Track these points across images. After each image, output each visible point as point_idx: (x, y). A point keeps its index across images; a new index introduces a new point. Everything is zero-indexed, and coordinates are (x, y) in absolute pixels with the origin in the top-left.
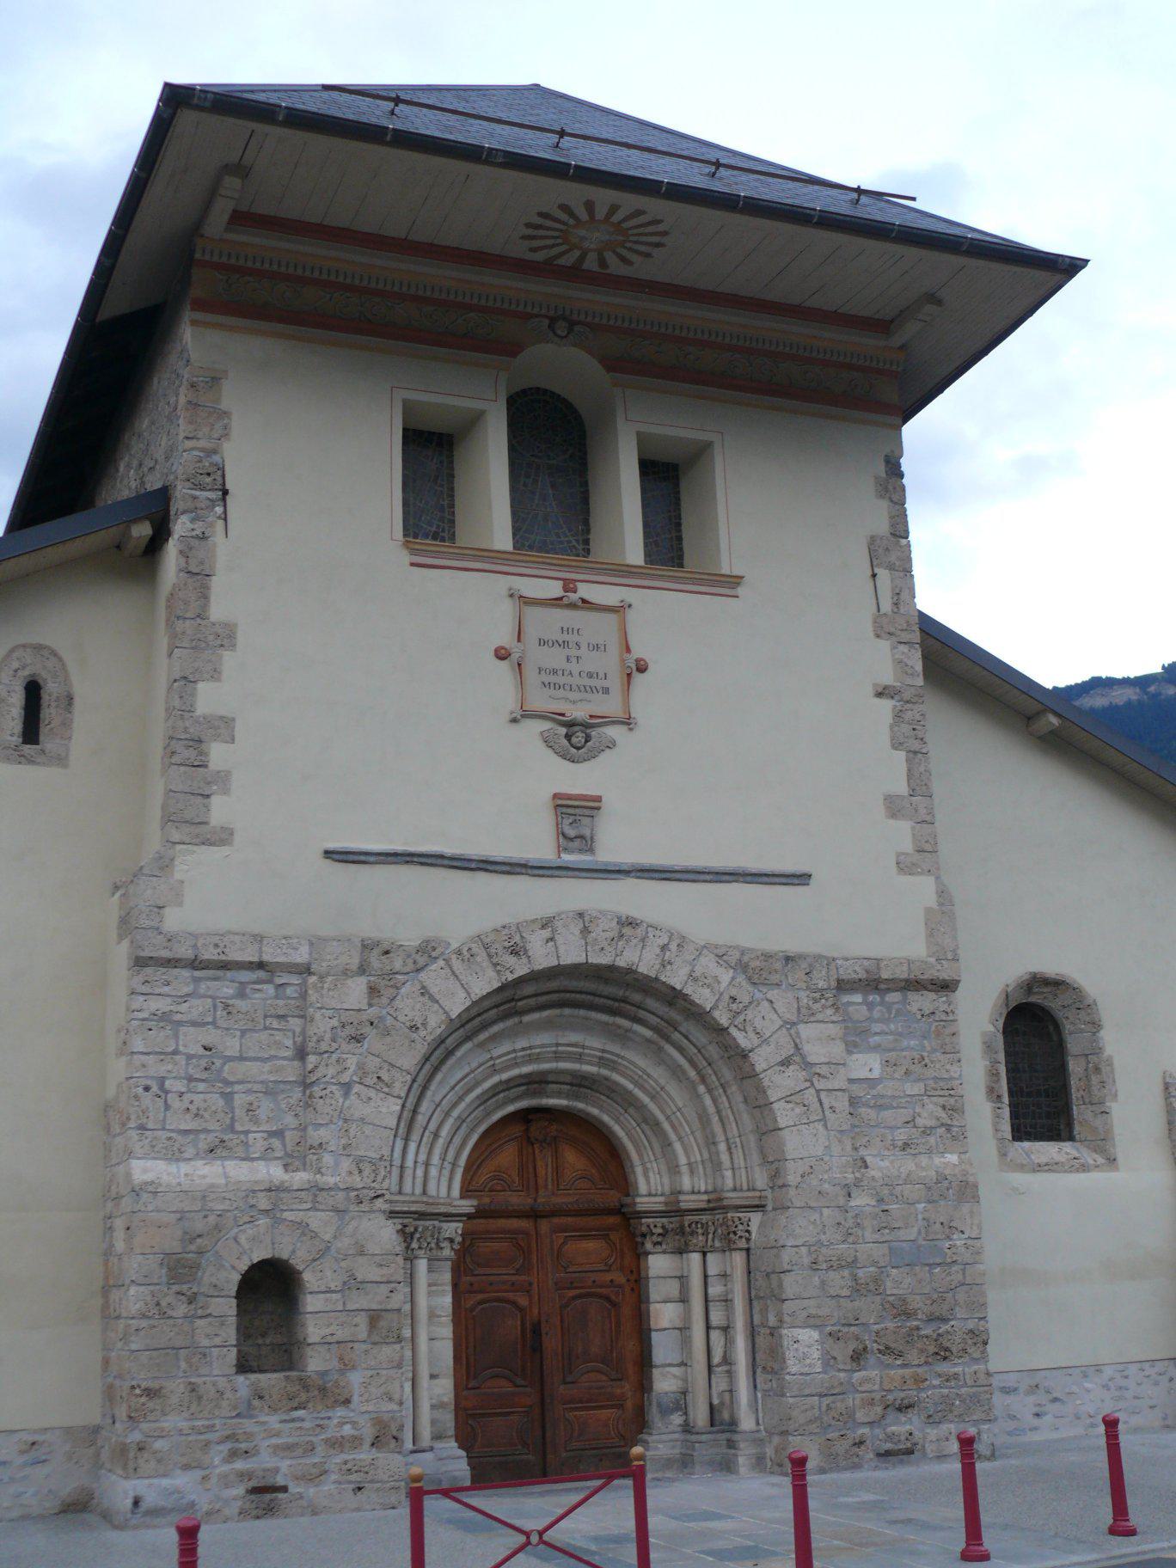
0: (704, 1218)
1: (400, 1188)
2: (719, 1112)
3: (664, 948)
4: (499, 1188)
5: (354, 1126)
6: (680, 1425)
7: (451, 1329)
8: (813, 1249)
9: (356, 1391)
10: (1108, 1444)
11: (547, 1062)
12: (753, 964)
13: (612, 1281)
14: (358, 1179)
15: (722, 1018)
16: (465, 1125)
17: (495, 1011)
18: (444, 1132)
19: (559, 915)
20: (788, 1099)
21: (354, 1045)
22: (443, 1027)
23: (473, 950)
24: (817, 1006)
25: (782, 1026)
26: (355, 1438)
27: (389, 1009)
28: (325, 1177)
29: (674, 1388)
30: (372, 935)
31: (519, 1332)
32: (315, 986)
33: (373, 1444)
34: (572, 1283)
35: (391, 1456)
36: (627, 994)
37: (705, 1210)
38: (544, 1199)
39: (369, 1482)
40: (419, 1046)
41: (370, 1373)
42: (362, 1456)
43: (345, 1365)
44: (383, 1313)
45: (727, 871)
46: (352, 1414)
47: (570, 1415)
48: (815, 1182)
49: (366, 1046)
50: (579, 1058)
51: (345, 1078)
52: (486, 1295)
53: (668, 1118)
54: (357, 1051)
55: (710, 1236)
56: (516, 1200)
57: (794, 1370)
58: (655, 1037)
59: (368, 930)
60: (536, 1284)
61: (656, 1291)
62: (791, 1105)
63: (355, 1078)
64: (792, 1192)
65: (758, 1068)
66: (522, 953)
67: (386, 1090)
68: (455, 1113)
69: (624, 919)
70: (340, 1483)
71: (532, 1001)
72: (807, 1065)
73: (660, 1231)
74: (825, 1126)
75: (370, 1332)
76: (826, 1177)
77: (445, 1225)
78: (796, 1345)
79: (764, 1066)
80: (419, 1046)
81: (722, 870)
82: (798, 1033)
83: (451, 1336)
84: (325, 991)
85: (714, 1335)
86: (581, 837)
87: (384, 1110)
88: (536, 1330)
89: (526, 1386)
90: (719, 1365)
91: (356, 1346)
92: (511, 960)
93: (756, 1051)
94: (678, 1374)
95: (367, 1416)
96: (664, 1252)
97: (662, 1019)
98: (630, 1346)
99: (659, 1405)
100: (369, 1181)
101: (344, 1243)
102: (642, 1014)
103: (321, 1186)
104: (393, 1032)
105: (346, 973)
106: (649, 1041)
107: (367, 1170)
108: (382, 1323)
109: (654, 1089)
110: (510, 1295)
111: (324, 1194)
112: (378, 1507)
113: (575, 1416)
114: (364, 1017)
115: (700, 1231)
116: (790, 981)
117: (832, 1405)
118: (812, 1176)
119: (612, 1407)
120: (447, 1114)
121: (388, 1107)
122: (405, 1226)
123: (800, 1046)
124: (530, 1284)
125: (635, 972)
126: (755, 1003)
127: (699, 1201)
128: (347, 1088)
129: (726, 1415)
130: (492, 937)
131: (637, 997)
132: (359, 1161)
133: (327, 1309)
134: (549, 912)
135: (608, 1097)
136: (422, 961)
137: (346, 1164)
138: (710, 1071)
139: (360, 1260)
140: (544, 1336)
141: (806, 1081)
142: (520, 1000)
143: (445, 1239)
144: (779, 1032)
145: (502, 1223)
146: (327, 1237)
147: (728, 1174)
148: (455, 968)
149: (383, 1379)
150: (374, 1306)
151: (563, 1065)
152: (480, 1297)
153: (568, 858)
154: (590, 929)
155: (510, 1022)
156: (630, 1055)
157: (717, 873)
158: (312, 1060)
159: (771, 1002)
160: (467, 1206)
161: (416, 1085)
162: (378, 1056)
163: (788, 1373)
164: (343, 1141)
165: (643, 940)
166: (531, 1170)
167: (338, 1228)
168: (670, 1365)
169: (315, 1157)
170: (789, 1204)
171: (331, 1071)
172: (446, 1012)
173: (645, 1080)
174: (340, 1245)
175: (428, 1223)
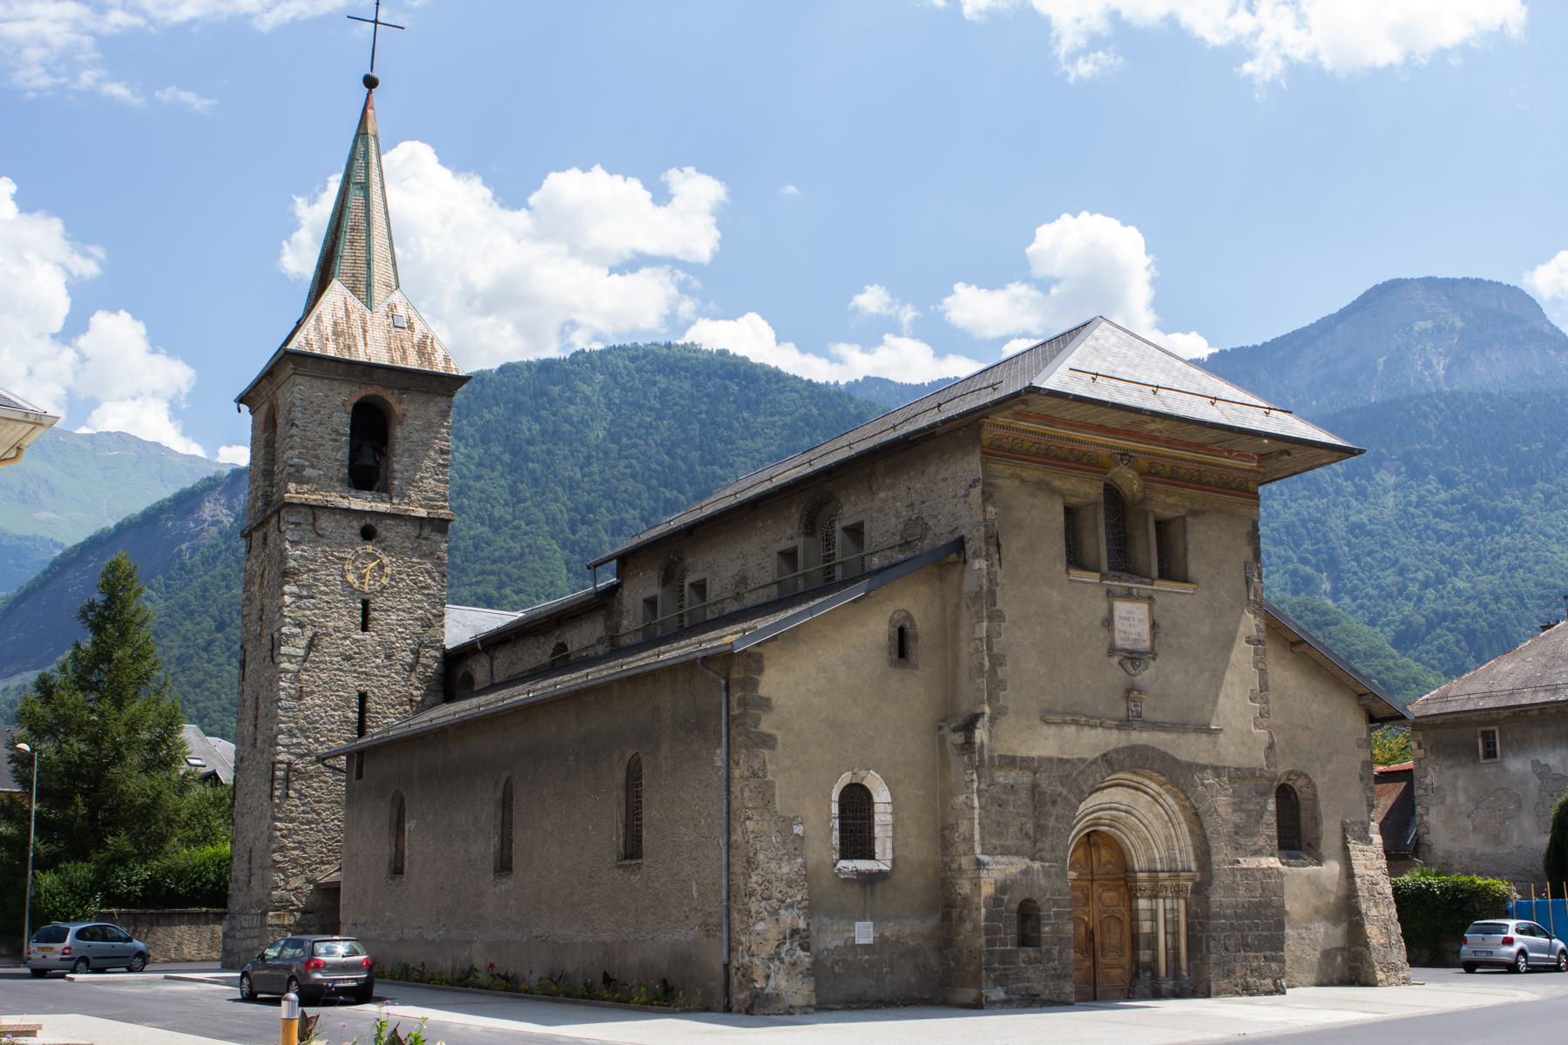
88: (1092, 933)
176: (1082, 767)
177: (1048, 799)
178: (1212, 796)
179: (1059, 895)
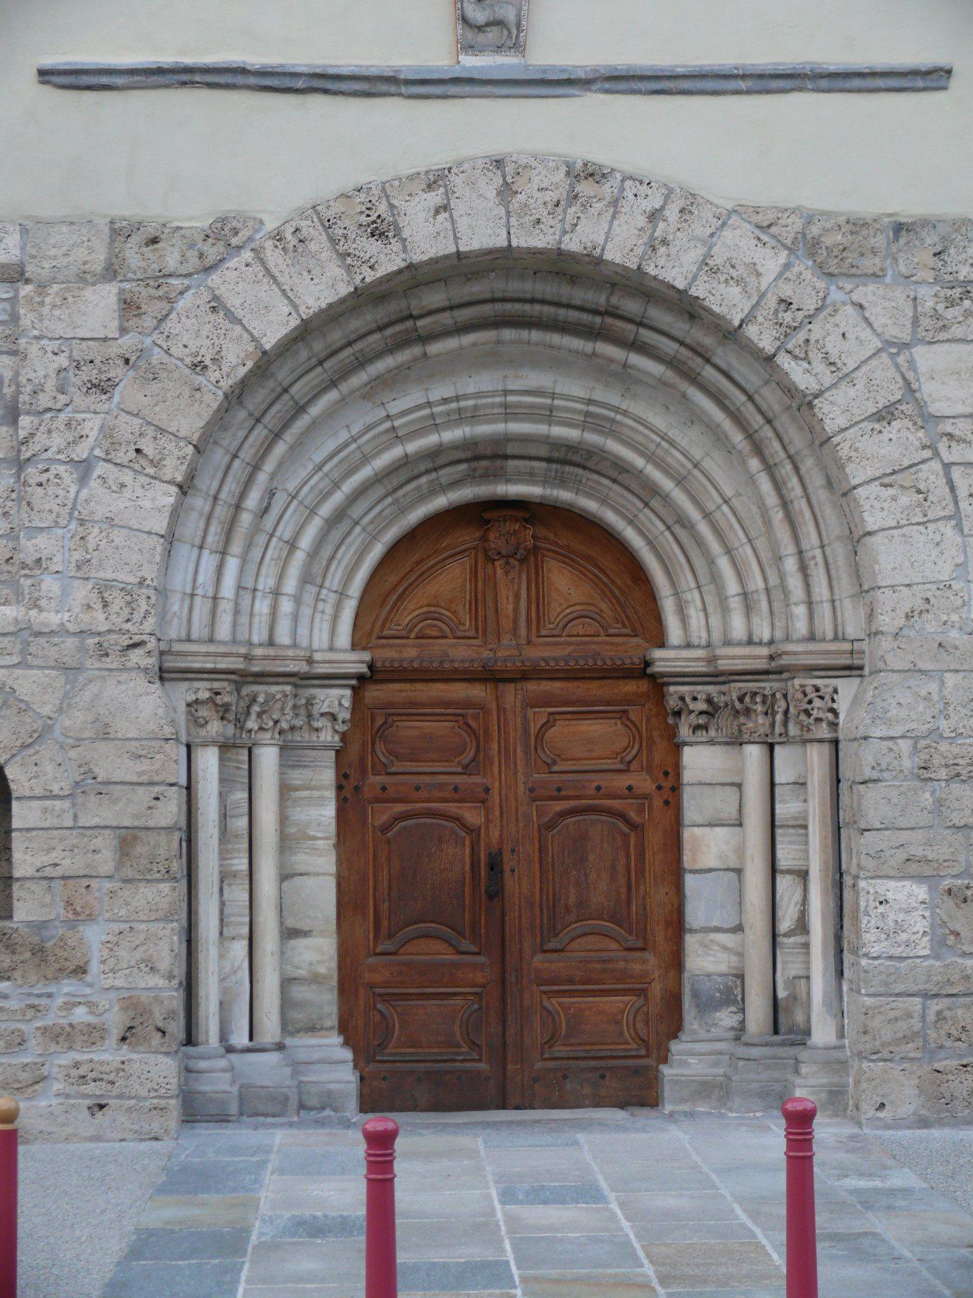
0: (768, 686)
1: (212, 631)
2: (785, 504)
3: (654, 216)
4: (435, 633)
5: (96, 531)
6: (733, 1028)
7: (333, 858)
8: (922, 743)
9: (96, 955)
10: (790, 1159)
11: (489, 422)
12: (828, 240)
13: (630, 788)
14: (102, 617)
15: (763, 336)
17: (377, 336)
19: (460, 164)
20: (887, 480)
21: (94, 399)
22: (250, 364)
23: (304, 231)
24: (950, 314)
25: (879, 351)
26: (92, 1028)
27: (155, 336)
28: (44, 615)
29: (723, 968)
30: (127, 212)
31: (468, 867)
32: (29, 300)
33: (124, 1039)
34: (559, 790)
35: (152, 1058)
36: (614, 300)
37: (767, 672)
38: (504, 652)
39: (117, 1097)
40: (208, 398)
41: (116, 927)
42: (106, 1057)
43: (76, 913)
44: (142, 834)
45: (781, 69)
46: (88, 991)
47: (553, 1003)
48: (930, 628)
49: (116, 399)
50: (549, 415)
51: (81, 452)
52: (408, 807)
53: (707, 516)
54: (100, 407)
55: (779, 717)
56: (461, 653)
57: (875, 950)
58: (670, 375)
59: (126, 209)
60: (496, 790)
61: (694, 806)
62: (891, 491)
63: (97, 452)
64: (886, 643)
65: (830, 427)
66: (390, 234)
67: (151, 471)
69: (579, 165)
70: (68, 1096)
71: (446, 319)
72: (926, 419)
73: (702, 706)
74: (959, 527)
75: (119, 865)
76: (955, 617)
77: (320, 693)
78: (881, 909)
79: (842, 421)
80: (208, 398)
81: (770, 70)
82: (911, 363)
83: (333, 869)
84: (46, 310)
85: (783, 883)
86: (499, 23)
87: (147, 504)
88: (495, 864)
89: (479, 954)
90: (788, 934)
91: (94, 883)
92: (371, 247)
93: (827, 395)
94: (730, 945)
95: (113, 995)
96: (712, 742)
97: (682, 343)
98: (659, 895)
99: (696, 995)
100: (120, 620)
101: (77, 719)
102: (647, 336)
103: (36, 628)
104: (163, 375)
105: (84, 278)
106: (662, 382)
107: (118, 601)
108: (139, 849)
109: (683, 466)
110: (451, 808)
111: (42, 640)
112: (130, 1136)
113: (560, 1004)
114: (113, 350)
115: (759, 708)
116: (902, 268)
117: (947, 1014)
118: (930, 616)
119: (625, 992)
121: (154, 499)
122: (217, 694)
123: (915, 386)
124: (487, 790)
125: (599, 261)
126: (829, 310)
127: (756, 657)
128: (84, 468)
129: (799, 1018)
130: (337, 208)
131: (631, 306)
132: (103, 588)
133: (46, 825)
134: (440, 159)
135: (614, 481)
136: (213, 253)
137: (81, 592)
138: (770, 434)
139: (102, 746)
140: (507, 875)
141: (924, 447)
142: (421, 317)
143: (322, 715)
144: (874, 362)
145: (438, 690)
146: (47, 710)
147: (800, 611)
148: (271, 264)
149: (142, 937)
150: (127, 822)
151: (516, 427)
152: (399, 808)
153: (473, 63)
154: (515, 187)
155: (404, 356)
156: (638, 408)
157: (761, 76)
158: (25, 421)
159: (861, 306)
160: (355, 662)
162: (137, 415)
163: (866, 955)
164: (77, 556)
165: (615, 203)
166: (490, 603)
167: (66, 695)
168: (717, 930)
169: (29, 582)
170: (881, 665)
171: (57, 441)
172: (254, 339)
173: (666, 451)
174: (67, 723)
175: (274, 689)
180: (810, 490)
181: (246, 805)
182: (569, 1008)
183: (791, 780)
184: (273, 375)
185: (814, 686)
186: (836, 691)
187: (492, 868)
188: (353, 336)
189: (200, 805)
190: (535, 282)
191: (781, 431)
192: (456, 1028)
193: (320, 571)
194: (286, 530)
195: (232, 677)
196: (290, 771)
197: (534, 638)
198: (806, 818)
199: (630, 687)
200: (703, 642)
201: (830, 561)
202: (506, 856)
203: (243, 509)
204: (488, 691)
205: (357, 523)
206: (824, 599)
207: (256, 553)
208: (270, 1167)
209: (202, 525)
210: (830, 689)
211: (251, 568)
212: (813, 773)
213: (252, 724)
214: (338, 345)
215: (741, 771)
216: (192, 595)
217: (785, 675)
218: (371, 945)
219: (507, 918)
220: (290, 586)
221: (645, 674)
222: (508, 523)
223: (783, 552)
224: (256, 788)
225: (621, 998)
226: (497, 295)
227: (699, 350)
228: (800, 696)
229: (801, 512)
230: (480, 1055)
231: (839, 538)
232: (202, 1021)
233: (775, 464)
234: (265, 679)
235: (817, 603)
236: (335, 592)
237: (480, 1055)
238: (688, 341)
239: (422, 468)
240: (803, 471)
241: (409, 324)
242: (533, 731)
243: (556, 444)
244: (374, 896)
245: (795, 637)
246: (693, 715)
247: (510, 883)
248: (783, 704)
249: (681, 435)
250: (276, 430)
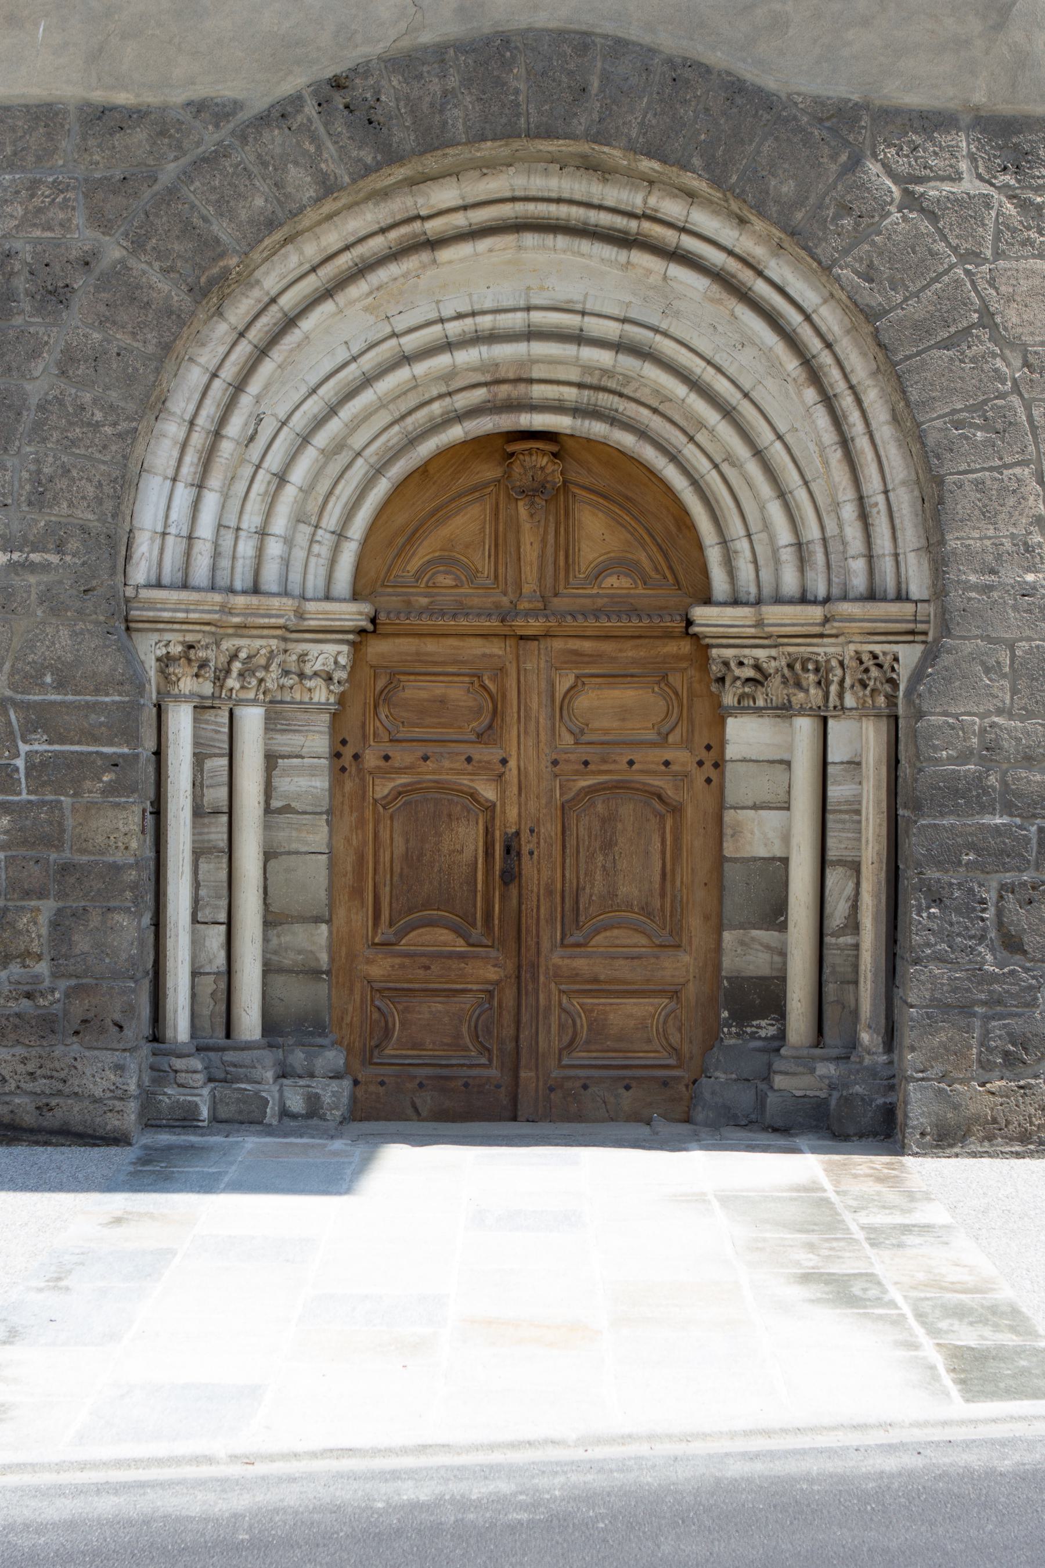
1: (187, 575)
16: (360, 461)
18: (298, 475)
36: (652, 201)
55: (834, 689)
68: (321, 439)
71: (459, 221)
73: (750, 673)
77: (314, 649)
85: (833, 877)
90: (842, 931)
115: (812, 677)
120: (305, 440)
122: (191, 647)
124: (504, 762)
135: (655, 411)
140: (525, 857)
143: (316, 674)
161: (217, 384)
176: (211, 138)
177: (21, 284)
178: (973, 256)
179: (60, 685)
180: (874, 425)
181: (226, 773)
182: (592, 1011)
183: (845, 759)
184: (258, 282)
185: (871, 652)
186: (896, 659)
187: (508, 850)
188: (352, 239)
189: (170, 773)
190: (560, 178)
191: (842, 357)
192: (464, 1029)
193: (316, 509)
194: (274, 461)
195: (207, 628)
196: (278, 736)
197: (562, 590)
198: (860, 803)
199: (672, 648)
200: (752, 598)
201: (895, 509)
202: (525, 836)
203: (223, 437)
204: (508, 649)
205: (359, 454)
206: (887, 552)
207: (240, 487)
208: (226, 1179)
209: (176, 454)
210: (889, 658)
211: (234, 504)
212: (868, 752)
213: (232, 682)
214: (335, 248)
215: (791, 748)
216: (164, 534)
217: (841, 639)
218: (370, 934)
219: (524, 907)
220: (279, 525)
221: (687, 634)
222: (534, 458)
223: (841, 497)
224: (237, 756)
225: (651, 1000)
226: (518, 193)
227: (750, 260)
228: (854, 664)
229: (863, 452)
230: (490, 1060)
231: (904, 483)
232: (169, 1015)
233: (835, 395)
234: (246, 632)
235: (878, 556)
236: (333, 533)
237: (490, 1060)
238: (737, 250)
239: (435, 392)
240: (866, 405)
241: (417, 226)
242: (558, 697)
243: (589, 367)
244: (374, 879)
245: (851, 595)
246: (738, 683)
247: (528, 867)
248: (839, 672)
249: (730, 359)
250: (262, 345)
